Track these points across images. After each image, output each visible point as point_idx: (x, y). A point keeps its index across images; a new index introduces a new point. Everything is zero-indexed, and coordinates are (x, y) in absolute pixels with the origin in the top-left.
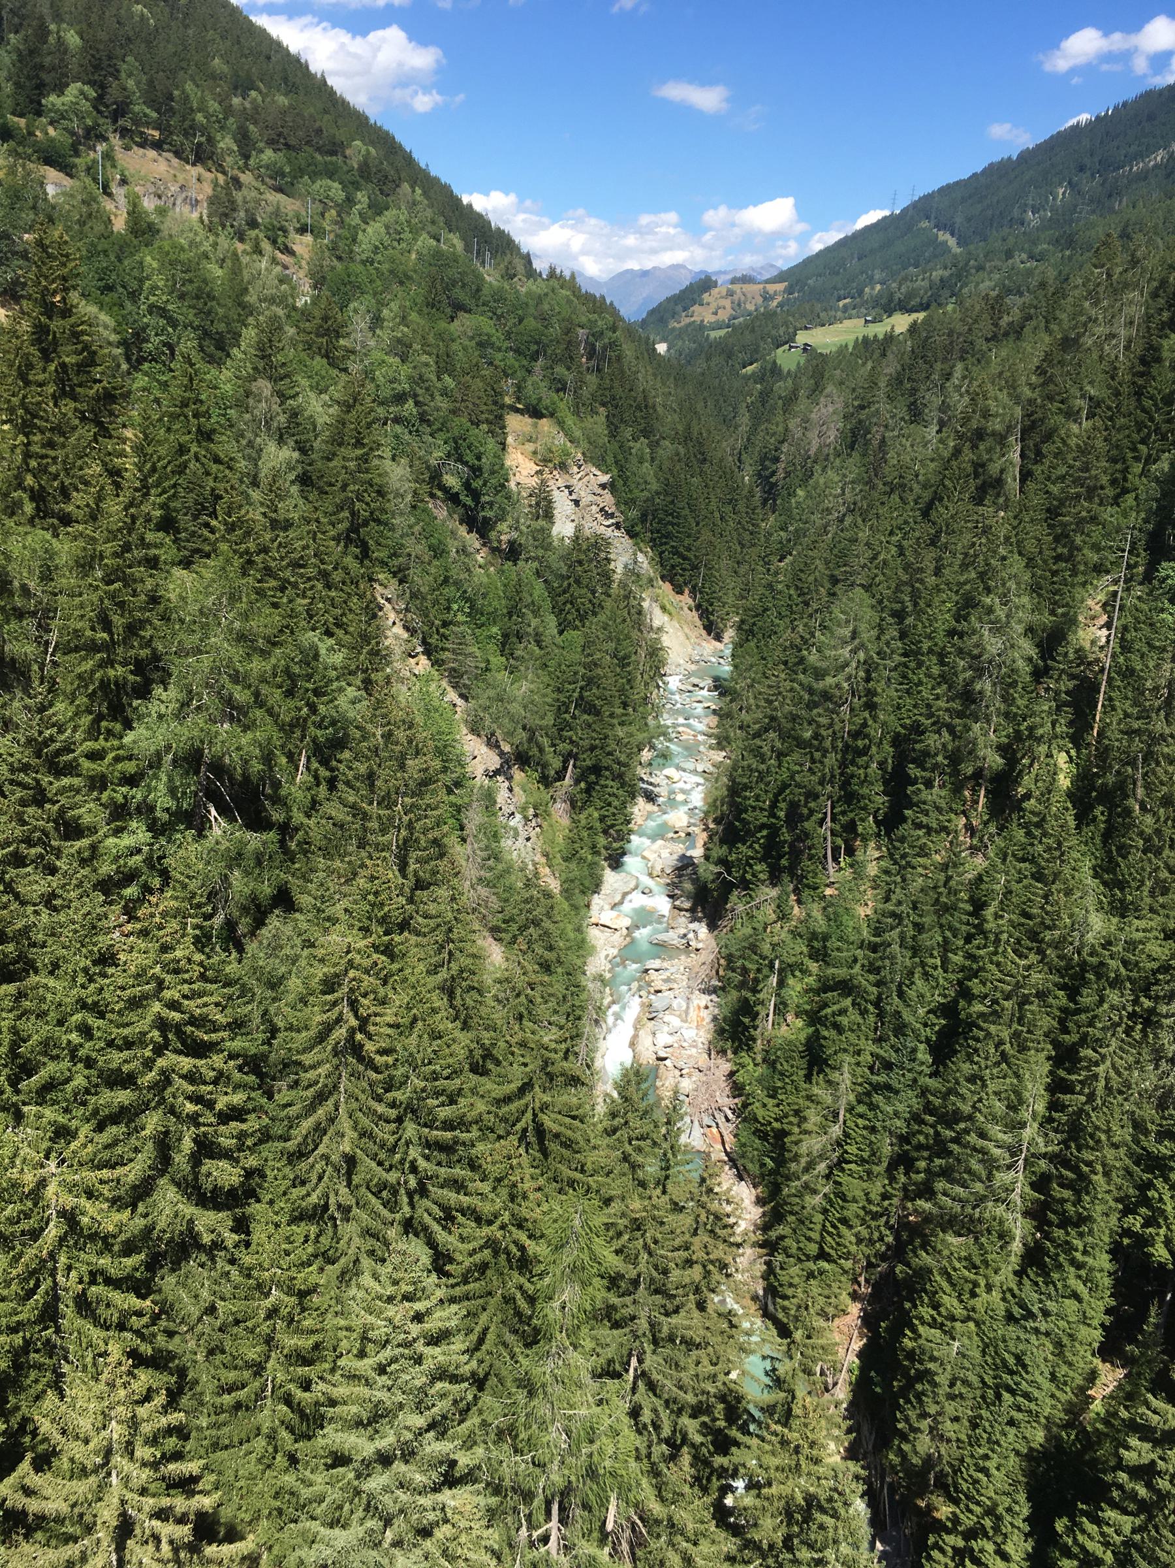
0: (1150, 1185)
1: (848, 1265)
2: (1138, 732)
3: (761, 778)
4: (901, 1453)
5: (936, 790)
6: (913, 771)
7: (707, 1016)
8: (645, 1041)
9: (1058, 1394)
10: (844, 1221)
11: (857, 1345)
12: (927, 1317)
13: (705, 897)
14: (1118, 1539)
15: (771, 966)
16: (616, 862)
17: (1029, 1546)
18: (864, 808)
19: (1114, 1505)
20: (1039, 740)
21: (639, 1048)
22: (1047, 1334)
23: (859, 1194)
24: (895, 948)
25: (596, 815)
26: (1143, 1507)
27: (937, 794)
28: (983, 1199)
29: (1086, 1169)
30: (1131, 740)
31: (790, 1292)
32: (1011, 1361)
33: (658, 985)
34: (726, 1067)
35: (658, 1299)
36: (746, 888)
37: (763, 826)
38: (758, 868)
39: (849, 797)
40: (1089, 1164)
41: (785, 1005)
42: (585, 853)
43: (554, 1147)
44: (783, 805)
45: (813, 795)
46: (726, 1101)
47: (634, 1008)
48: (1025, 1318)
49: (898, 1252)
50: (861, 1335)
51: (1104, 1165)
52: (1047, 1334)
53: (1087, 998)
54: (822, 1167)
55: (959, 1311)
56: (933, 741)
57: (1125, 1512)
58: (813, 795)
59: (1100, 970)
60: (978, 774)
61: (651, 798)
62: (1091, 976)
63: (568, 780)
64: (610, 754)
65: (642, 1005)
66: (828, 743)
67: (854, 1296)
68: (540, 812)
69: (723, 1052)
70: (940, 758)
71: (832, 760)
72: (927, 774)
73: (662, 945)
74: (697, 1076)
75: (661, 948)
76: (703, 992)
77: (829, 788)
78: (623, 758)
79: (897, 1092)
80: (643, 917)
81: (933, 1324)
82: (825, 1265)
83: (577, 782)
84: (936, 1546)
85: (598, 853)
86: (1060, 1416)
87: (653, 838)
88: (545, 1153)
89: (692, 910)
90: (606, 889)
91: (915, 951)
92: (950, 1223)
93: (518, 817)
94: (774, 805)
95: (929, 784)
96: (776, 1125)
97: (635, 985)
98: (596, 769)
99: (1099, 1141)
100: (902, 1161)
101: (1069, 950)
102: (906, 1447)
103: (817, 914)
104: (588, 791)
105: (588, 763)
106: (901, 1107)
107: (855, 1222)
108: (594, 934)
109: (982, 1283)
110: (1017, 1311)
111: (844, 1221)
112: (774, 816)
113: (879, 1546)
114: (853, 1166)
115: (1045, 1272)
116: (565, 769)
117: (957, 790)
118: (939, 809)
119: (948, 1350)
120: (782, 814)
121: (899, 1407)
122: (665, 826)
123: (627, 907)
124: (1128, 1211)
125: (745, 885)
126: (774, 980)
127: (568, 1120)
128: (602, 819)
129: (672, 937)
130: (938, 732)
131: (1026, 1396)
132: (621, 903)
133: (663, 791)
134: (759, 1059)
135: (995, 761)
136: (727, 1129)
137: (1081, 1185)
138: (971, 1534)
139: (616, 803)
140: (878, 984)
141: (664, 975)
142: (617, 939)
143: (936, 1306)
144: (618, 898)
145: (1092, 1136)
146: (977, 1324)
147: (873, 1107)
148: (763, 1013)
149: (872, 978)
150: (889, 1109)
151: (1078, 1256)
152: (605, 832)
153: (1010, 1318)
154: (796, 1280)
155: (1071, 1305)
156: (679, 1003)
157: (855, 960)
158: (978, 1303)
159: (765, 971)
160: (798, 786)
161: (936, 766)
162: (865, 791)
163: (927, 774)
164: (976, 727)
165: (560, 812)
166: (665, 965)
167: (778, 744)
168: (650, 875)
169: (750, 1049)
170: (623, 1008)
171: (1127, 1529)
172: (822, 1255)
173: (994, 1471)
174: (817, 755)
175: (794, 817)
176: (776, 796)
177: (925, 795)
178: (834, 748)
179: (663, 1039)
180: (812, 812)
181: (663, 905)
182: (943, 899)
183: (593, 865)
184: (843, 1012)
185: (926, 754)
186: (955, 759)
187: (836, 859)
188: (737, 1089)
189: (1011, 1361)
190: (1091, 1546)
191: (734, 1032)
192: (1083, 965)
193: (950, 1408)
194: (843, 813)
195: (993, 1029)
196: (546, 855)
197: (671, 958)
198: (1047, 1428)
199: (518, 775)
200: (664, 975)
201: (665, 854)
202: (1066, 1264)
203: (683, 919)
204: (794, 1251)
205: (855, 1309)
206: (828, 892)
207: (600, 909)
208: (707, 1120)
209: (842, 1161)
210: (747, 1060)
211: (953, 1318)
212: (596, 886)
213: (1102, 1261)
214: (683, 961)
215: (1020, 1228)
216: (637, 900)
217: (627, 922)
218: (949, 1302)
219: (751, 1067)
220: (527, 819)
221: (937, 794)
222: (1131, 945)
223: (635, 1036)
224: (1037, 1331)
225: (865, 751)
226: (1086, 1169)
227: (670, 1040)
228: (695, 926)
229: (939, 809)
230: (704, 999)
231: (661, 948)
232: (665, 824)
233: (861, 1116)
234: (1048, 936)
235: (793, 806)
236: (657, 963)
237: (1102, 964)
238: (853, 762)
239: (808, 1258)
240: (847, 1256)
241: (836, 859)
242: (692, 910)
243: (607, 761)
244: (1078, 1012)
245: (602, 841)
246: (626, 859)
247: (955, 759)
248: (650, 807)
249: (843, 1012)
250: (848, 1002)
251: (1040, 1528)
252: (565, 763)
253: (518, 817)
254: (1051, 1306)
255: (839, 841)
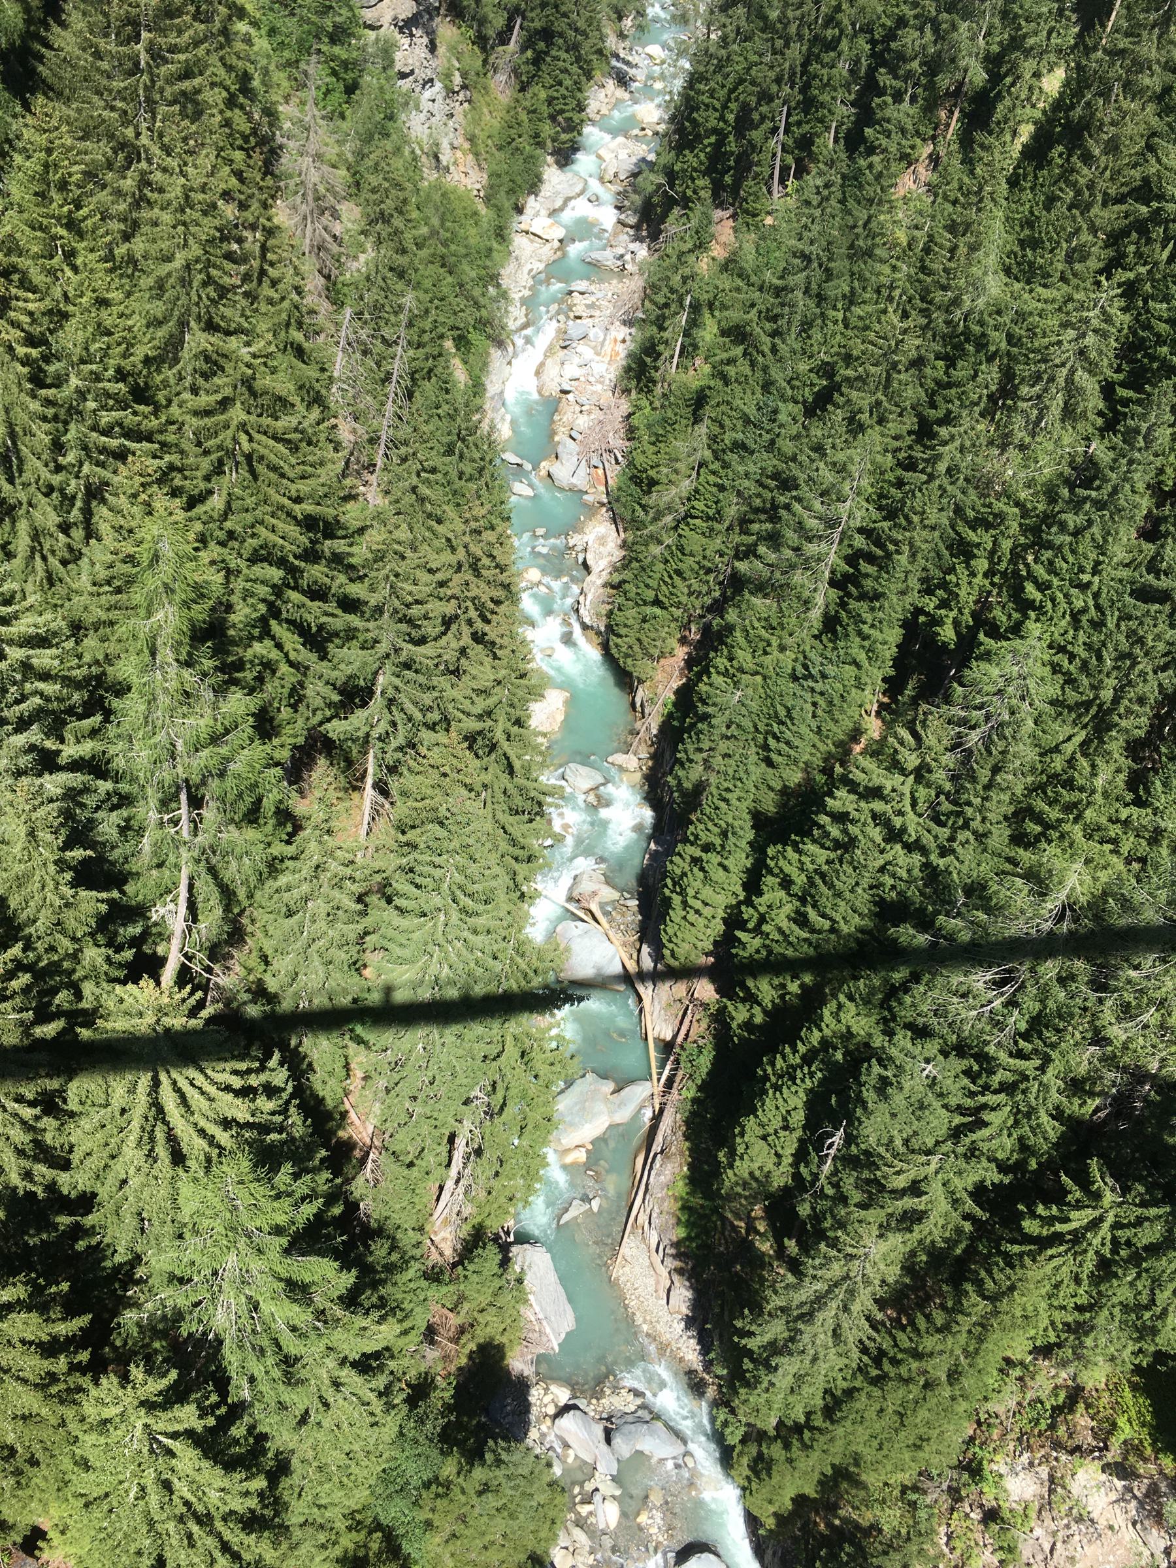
0: (952, 570)
1: (678, 613)
2: (1122, 53)
3: (719, 68)
4: (677, 778)
5: (905, 105)
6: (884, 78)
7: (622, 351)
8: (552, 370)
9: (819, 745)
10: (679, 573)
11: (676, 683)
12: (722, 668)
13: (649, 215)
14: (811, 867)
15: (681, 301)
16: (565, 156)
17: (748, 863)
18: (821, 121)
19: (814, 841)
20: (1027, 52)
21: (544, 377)
22: (822, 694)
23: (696, 548)
24: (799, 294)
25: (543, 95)
26: (837, 845)
27: (905, 112)
28: (793, 567)
29: (891, 547)
30: (1112, 64)
31: (623, 631)
32: (782, 713)
33: (579, 310)
34: (625, 407)
35: (404, 627)
36: (686, 207)
37: (715, 131)
38: (700, 183)
39: (808, 104)
40: (896, 543)
41: (695, 347)
42: (524, 143)
43: (261, 469)
44: (733, 106)
45: (766, 97)
46: (618, 442)
47: (549, 331)
48: (805, 678)
49: (718, 608)
50: (681, 675)
51: (911, 545)
52: (822, 694)
53: (962, 371)
54: (668, 519)
55: (749, 665)
56: (910, 39)
57: (823, 846)
58: (766, 97)
59: (981, 343)
60: (957, 92)
61: (623, 80)
62: (970, 348)
63: (513, 46)
64: (565, 15)
65: (559, 331)
66: (793, 29)
67: (683, 641)
68: (469, 87)
69: (627, 391)
70: (915, 65)
71: (796, 52)
72: (898, 84)
73: (595, 265)
74: (597, 414)
75: (593, 268)
76: (624, 323)
77: (787, 89)
78: (581, 24)
79: (752, 453)
80: (584, 229)
81: (726, 674)
82: (658, 611)
83: (523, 49)
84: (795, 845)
85: (540, 145)
86: (818, 762)
87: (614, 132)
88: (255, 477)
89: (637, 227)
90: (546, 190)
91: (820, 298)
92: (762, 588)
93: (438, 85)
94: (725, 107)
95: (898, 97)
96: (651, 473)
97: (554, 307)
98: (547, 34)
99: (910, 522)
100: (743, 523)
101: (958, 314)
102: (681, 773)
103: (749, 248)
104: (537, 61)
105: (537, 25)
106: (752, 468)
107: (688, 574)
108: (520, 243)
109: (775, 642)
110: (800, 671)
111: (679, 573)
112: (722, 118)
113: (653, 846)
114: (698, 522)
115: (835, 638)
116: (510, 29)
117: (930, 108)
118: (903, 131)
119: (728, 698)
120: (731, 117)
121: (683, 741)
122: (632, 120)
123: (567, 216)
124: (929, 592)
125: (686, 202)
126: (683, 318)
127: (271, 442)
128: (550, 101)
129: (607, 257)
130: (921, 29)
131: (787, 743)
132: (562, 209)
133: (640, 74)
134: (657, 404)
135: (978, 76)
136: (613, 471)
137: (883, 563)
138: (707, 848)
139: (568, 82)
140: (775, 334)
141: (589, 300)
142: (547, 252)
143: (731, 659)
144: (558, 203)
145: (906, 518)
146: (765, 678)
147: (726, 465)
148: (666, 354)
149: (768, 326)
150: (741, 469)
151: (865, 629)
152: (553, 118)
153: (795, 678)
154: (630, 622)
155: (850, 670)
156: (596, 333)
157: (753, 305)
158: (767, 660)
159: (674, 307)
160: (753, 83)
161: (909, 74)
162: (825, 98)
163: (898, 84)
164: (964, 26)
165: (500, 86)
166: (593, 288)
167: (743, 23)
168: (601, 179)
169: (650, 391)
170: (538, 330)
171: (821, 860)
172: (657, 602)
173: (734, 802)
174: (779, 43)
175: (744, 123)
176: (731, 91)
177: (892, 112)
178: (800, 37)
179: (571, 370)
180: (763, 118)
181: (608, 217)
182: (861, 243)
183: (530, 160)
184: (731, 361)
185: (902, 57)
186: (934, 66)
187: (782, 181)
188: (631, 433)
189: (782, 713)
190: (787, 869)
191: (640, 371)
192: (967, 333)
193: (723, 746)
194: (799, 124)
195: (854, 394)
196: (471, 139)
197: (601, 281)
198: (805, 771)
199: (447, 31)
200: (589, 300)
201: (623, 155)
202: (852, 633)
203: (625, 237)
204: (632, 595)
205: (681, 652)
206: (769, 221)
207: (536, 215)
208: (595, 461)
209: (688, 515)
210: (644, 403)
211: (741, 670)
212: (534, 185)
213: (894, 635)
214: (614, 286)
215: (823, 597)
216: (580, 209)
217: (560, 233)
218: (744, 656)
219: (647, 410)
220: (450, 92)
221: (905, 112)
222: (1021, 316)
223: (542, 364)
224: (813, 690)
225: (832, 45)
226: (891, 547)
227: (577, 373)
228: (635, 246)
229: (903, 131)
230: (622, 332)
231: (593, 268)
232: (633, 117)
233: (714, 473)
234: (939, 296)
235: (745, 110)
236: (581, 285)
237: (984, 335)
238: (818, 59)
239: (645, 603)
240: (678, 605)
241: (782, 181)
242: (637, 227)
243: (560, 25)
244: (949, 385)
245: (547, 129)
246: (579, 156)
247: (934, 66)
248: (620, 93)
249: (731, 361)
250: (739, 350)
251: (758, 848)
252: (511, 20)
253: (438, 85)
254: (830, 670)
255: (790, 160)
